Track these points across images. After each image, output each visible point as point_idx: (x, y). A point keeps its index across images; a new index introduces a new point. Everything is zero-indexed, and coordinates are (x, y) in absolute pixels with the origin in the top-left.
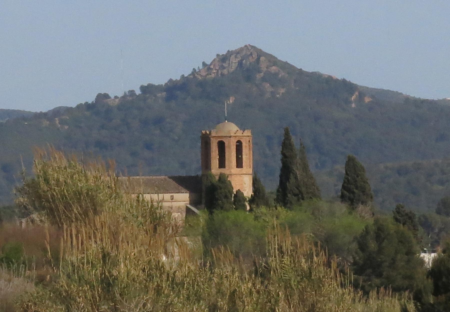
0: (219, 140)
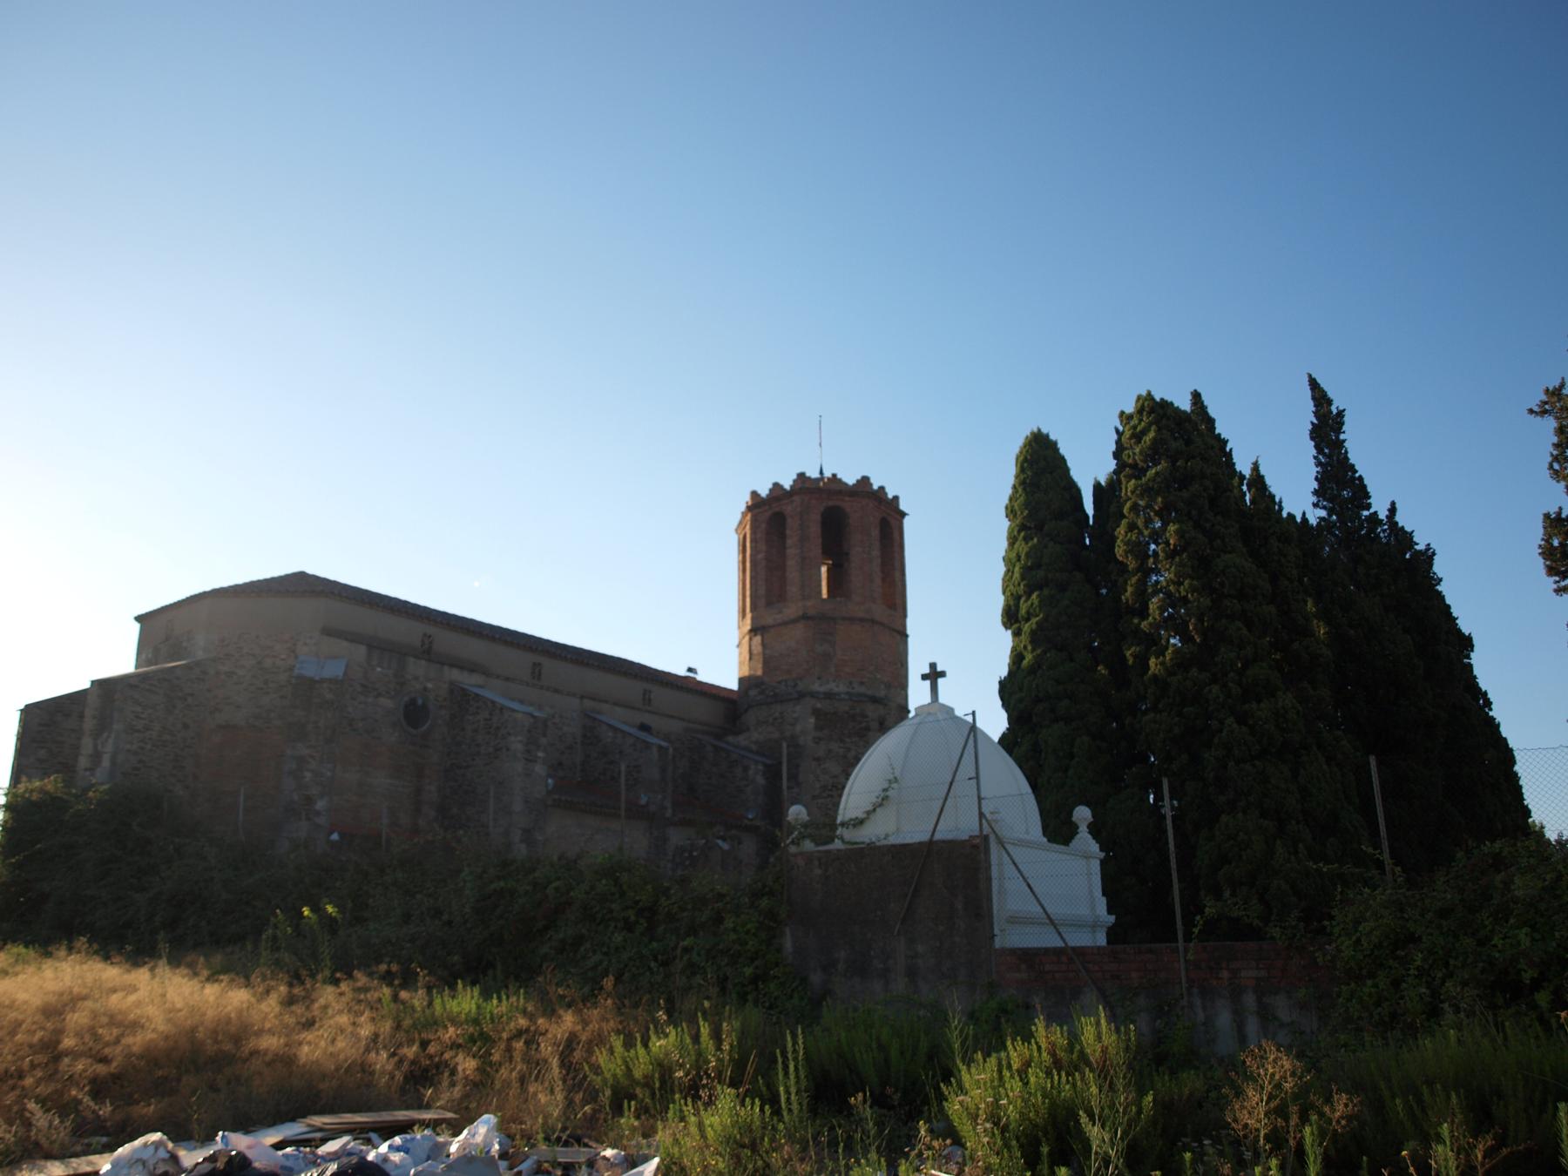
0: (831, 503)
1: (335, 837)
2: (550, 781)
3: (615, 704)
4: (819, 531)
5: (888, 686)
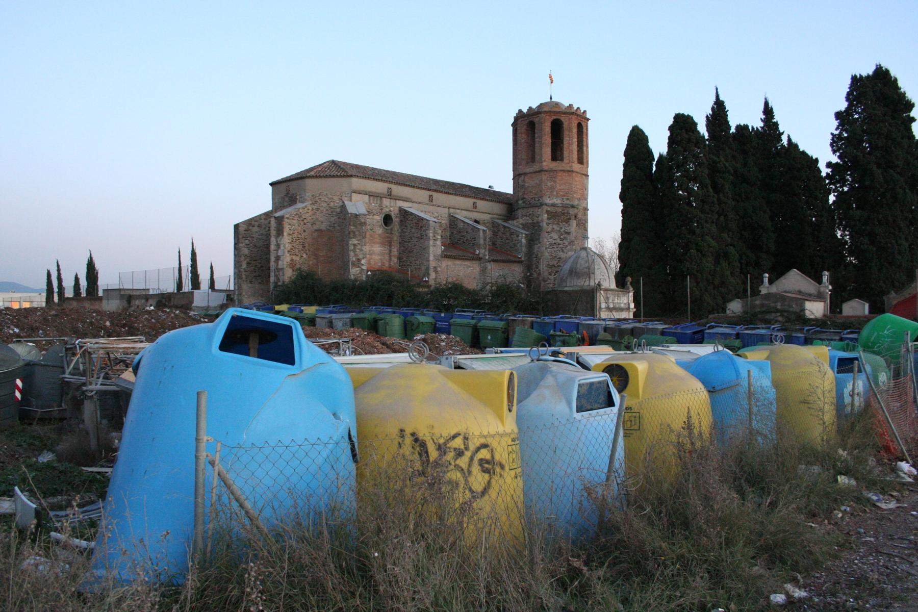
0: (555, 117)
1: (369, 273)
2: (443, 247)
3: (462, 210)
4: (550, 131)
5: (579, 200)
